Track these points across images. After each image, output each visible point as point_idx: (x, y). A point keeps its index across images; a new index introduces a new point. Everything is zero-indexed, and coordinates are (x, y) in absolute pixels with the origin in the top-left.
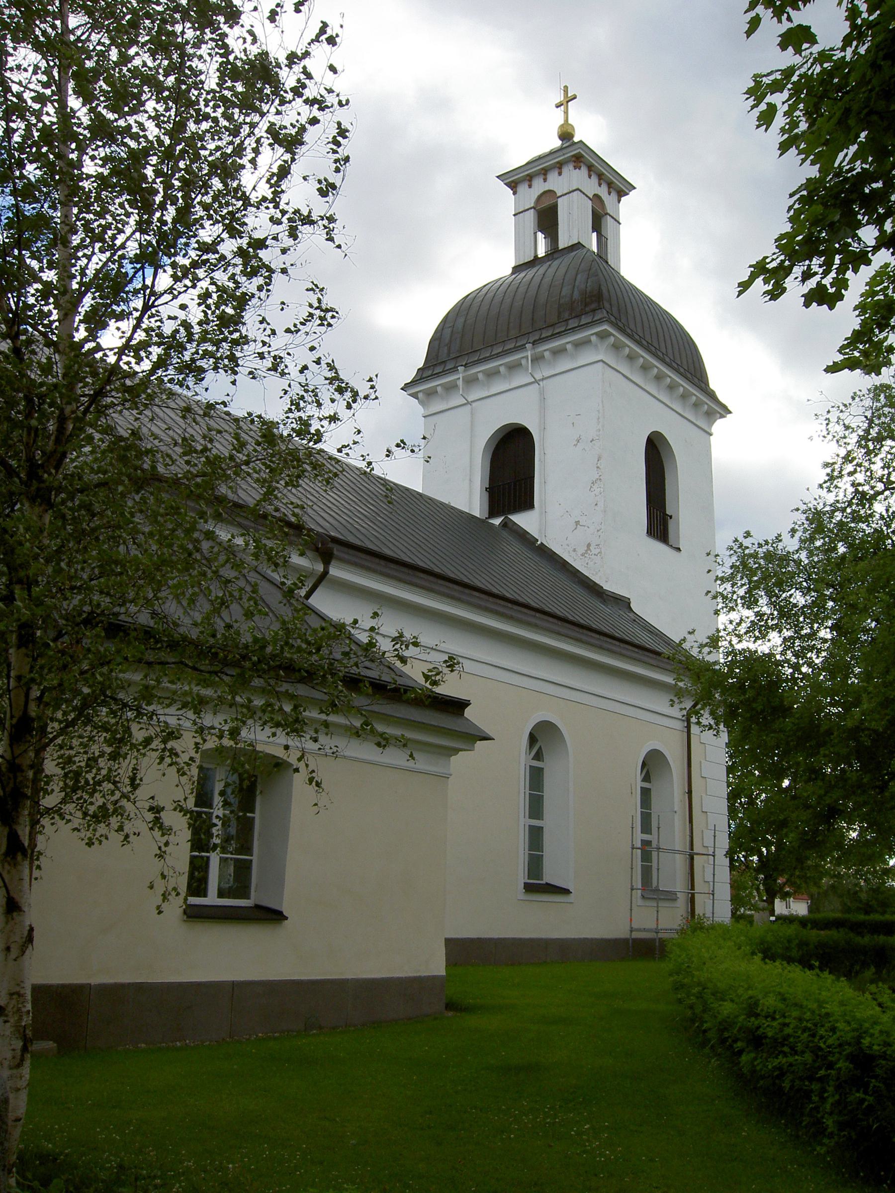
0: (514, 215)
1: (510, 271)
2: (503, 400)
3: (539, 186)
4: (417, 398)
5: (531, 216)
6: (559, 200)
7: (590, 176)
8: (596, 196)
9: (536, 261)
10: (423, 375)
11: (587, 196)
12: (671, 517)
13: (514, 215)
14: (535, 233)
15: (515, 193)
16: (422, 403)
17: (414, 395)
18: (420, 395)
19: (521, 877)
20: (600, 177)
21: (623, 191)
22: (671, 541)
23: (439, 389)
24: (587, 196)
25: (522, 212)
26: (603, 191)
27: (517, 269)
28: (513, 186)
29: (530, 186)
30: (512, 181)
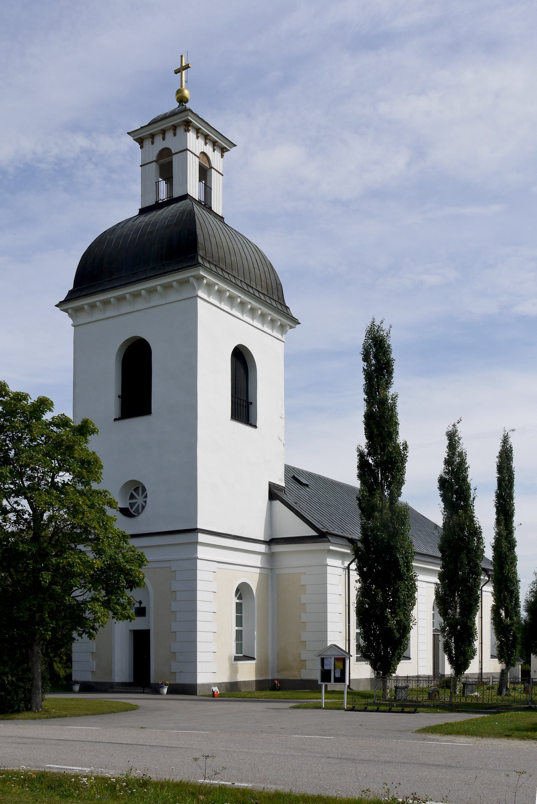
0: (141, 166)
1: (137, 212)
2: (133, 313)
3: (160, 144)
4: (67, 312)
5: (154, 168)
6: (174, 156)
7: (197, 137)
8: (203, 153)
9: (158, 206)
10: (72, 296)
11: (192, 153)
12: (251, 403)
13: (141, 166)
14: (157, 183)
15: (142, 147)
16: (70, 316)
17: (65, 311)
18: (70, 311)
19: (233, 651)
20: (206, 137)
21: (225, 148)
22: (251, 421)
23: (128, 296)
24: (192, 153)
25: (147, 164)
26: (208, 149)
27: (143, 211)
28: (141, 141)
29: (153, 143)
30: (140, 138)
